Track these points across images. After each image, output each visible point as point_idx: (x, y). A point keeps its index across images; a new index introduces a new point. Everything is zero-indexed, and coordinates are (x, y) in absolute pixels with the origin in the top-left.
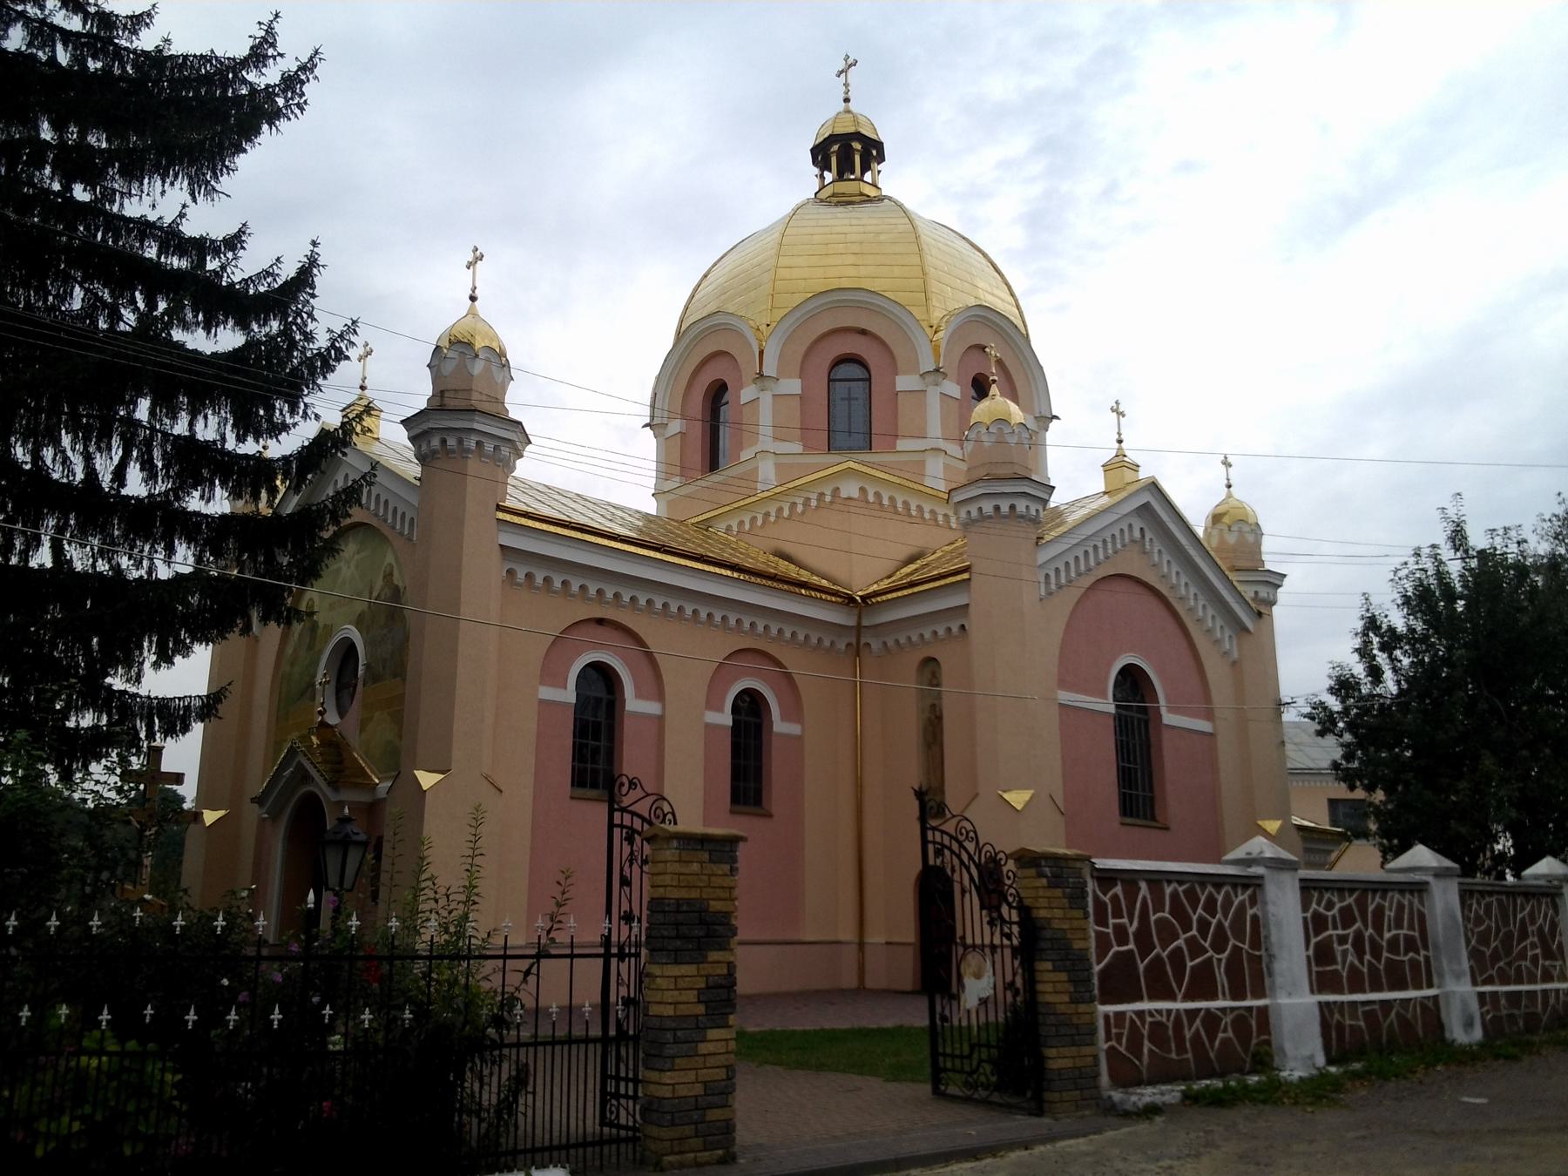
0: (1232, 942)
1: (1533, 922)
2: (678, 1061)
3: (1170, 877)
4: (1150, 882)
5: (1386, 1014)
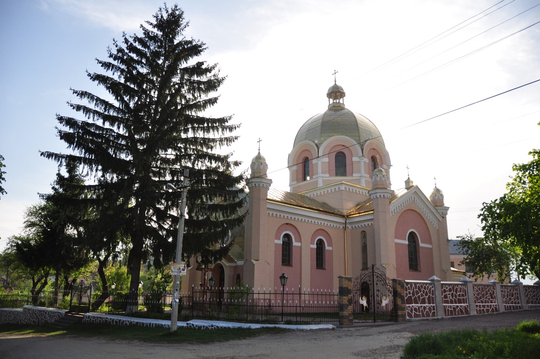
0: (429, 294)
3: (418, 283)
4: (414, 284)
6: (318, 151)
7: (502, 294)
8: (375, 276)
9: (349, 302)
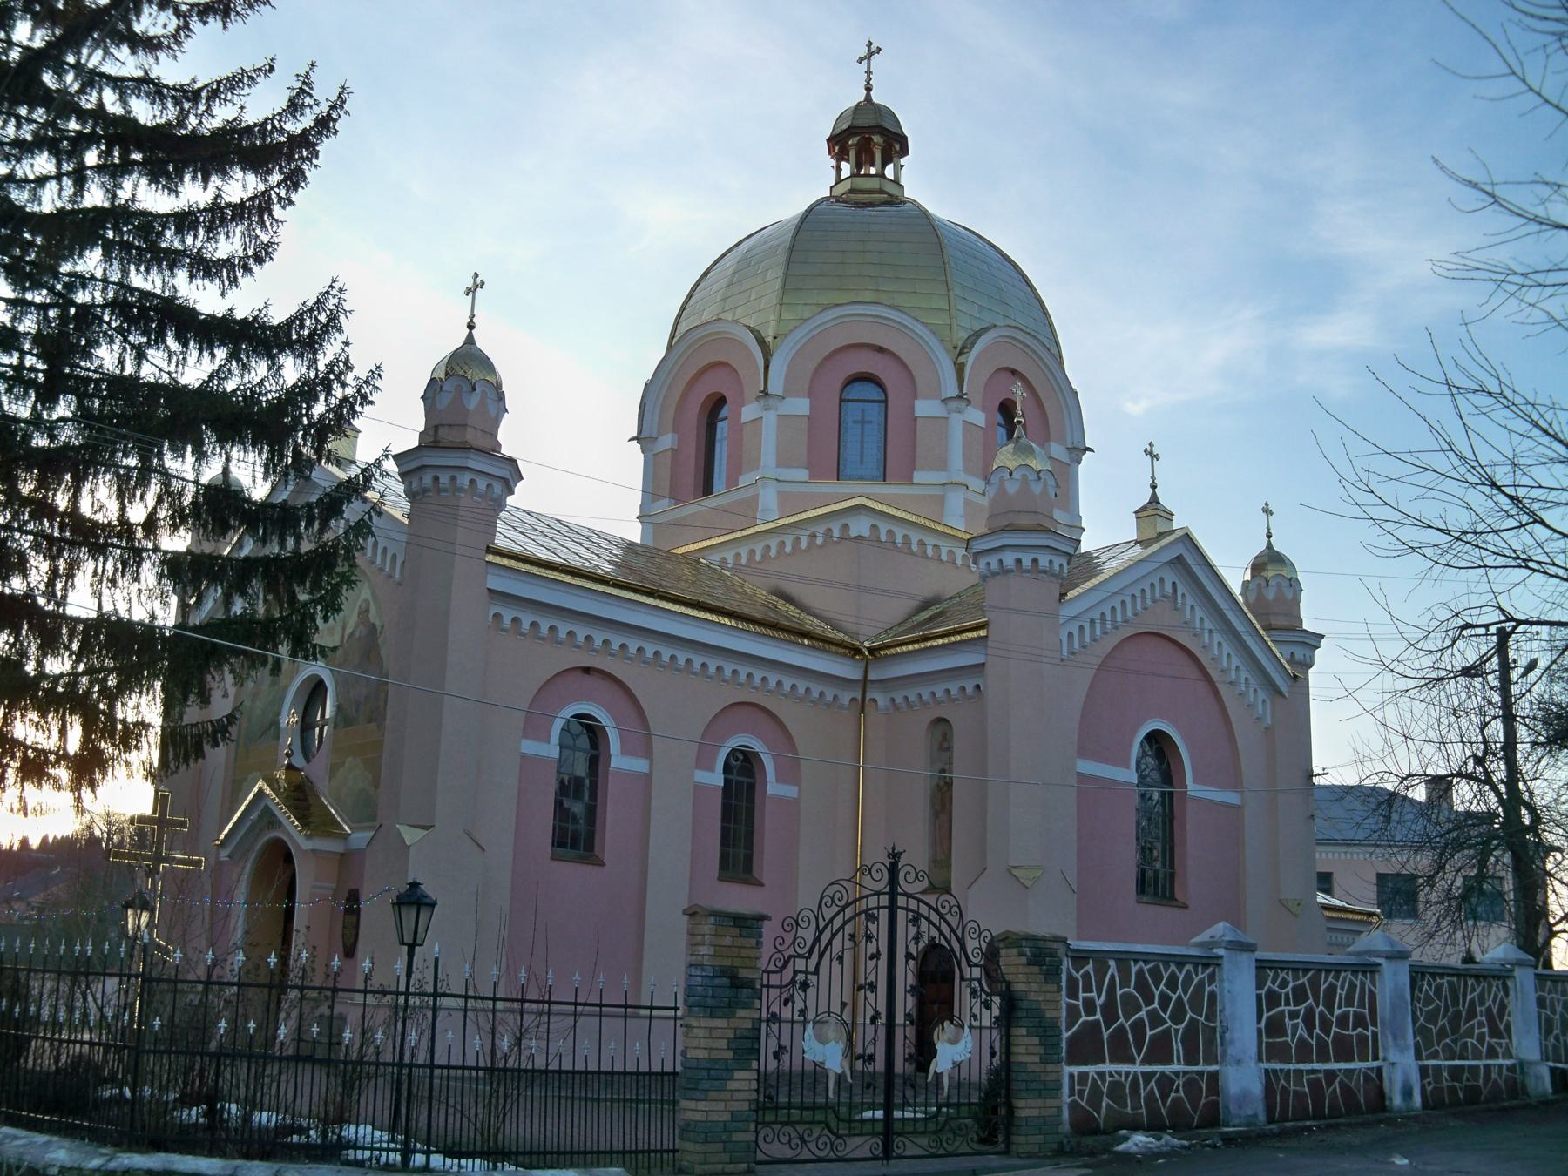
0: (1190, 1014)
1: (1482, 1003)
2: (711, 1093)
4: (1118, 961)
5: (1330, 1083)
6: (767, 367)
7: (1539, 1015)
8: (901, 914)
9: (735, 1050)
